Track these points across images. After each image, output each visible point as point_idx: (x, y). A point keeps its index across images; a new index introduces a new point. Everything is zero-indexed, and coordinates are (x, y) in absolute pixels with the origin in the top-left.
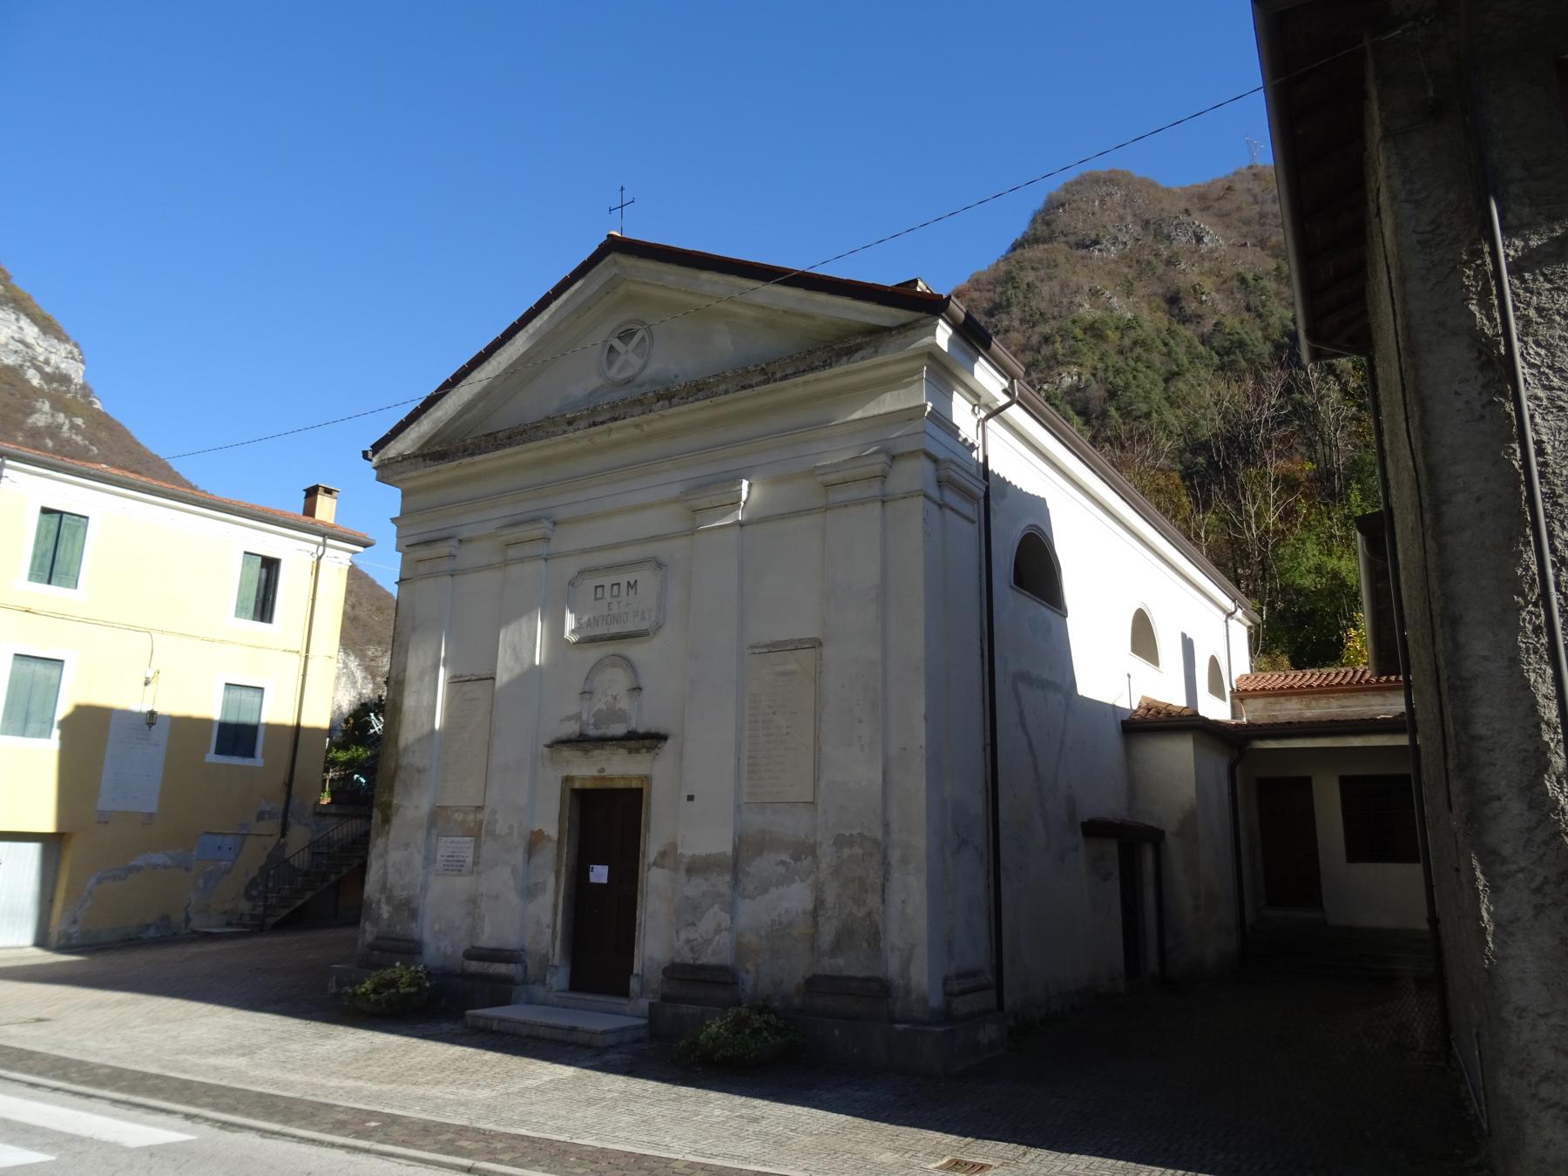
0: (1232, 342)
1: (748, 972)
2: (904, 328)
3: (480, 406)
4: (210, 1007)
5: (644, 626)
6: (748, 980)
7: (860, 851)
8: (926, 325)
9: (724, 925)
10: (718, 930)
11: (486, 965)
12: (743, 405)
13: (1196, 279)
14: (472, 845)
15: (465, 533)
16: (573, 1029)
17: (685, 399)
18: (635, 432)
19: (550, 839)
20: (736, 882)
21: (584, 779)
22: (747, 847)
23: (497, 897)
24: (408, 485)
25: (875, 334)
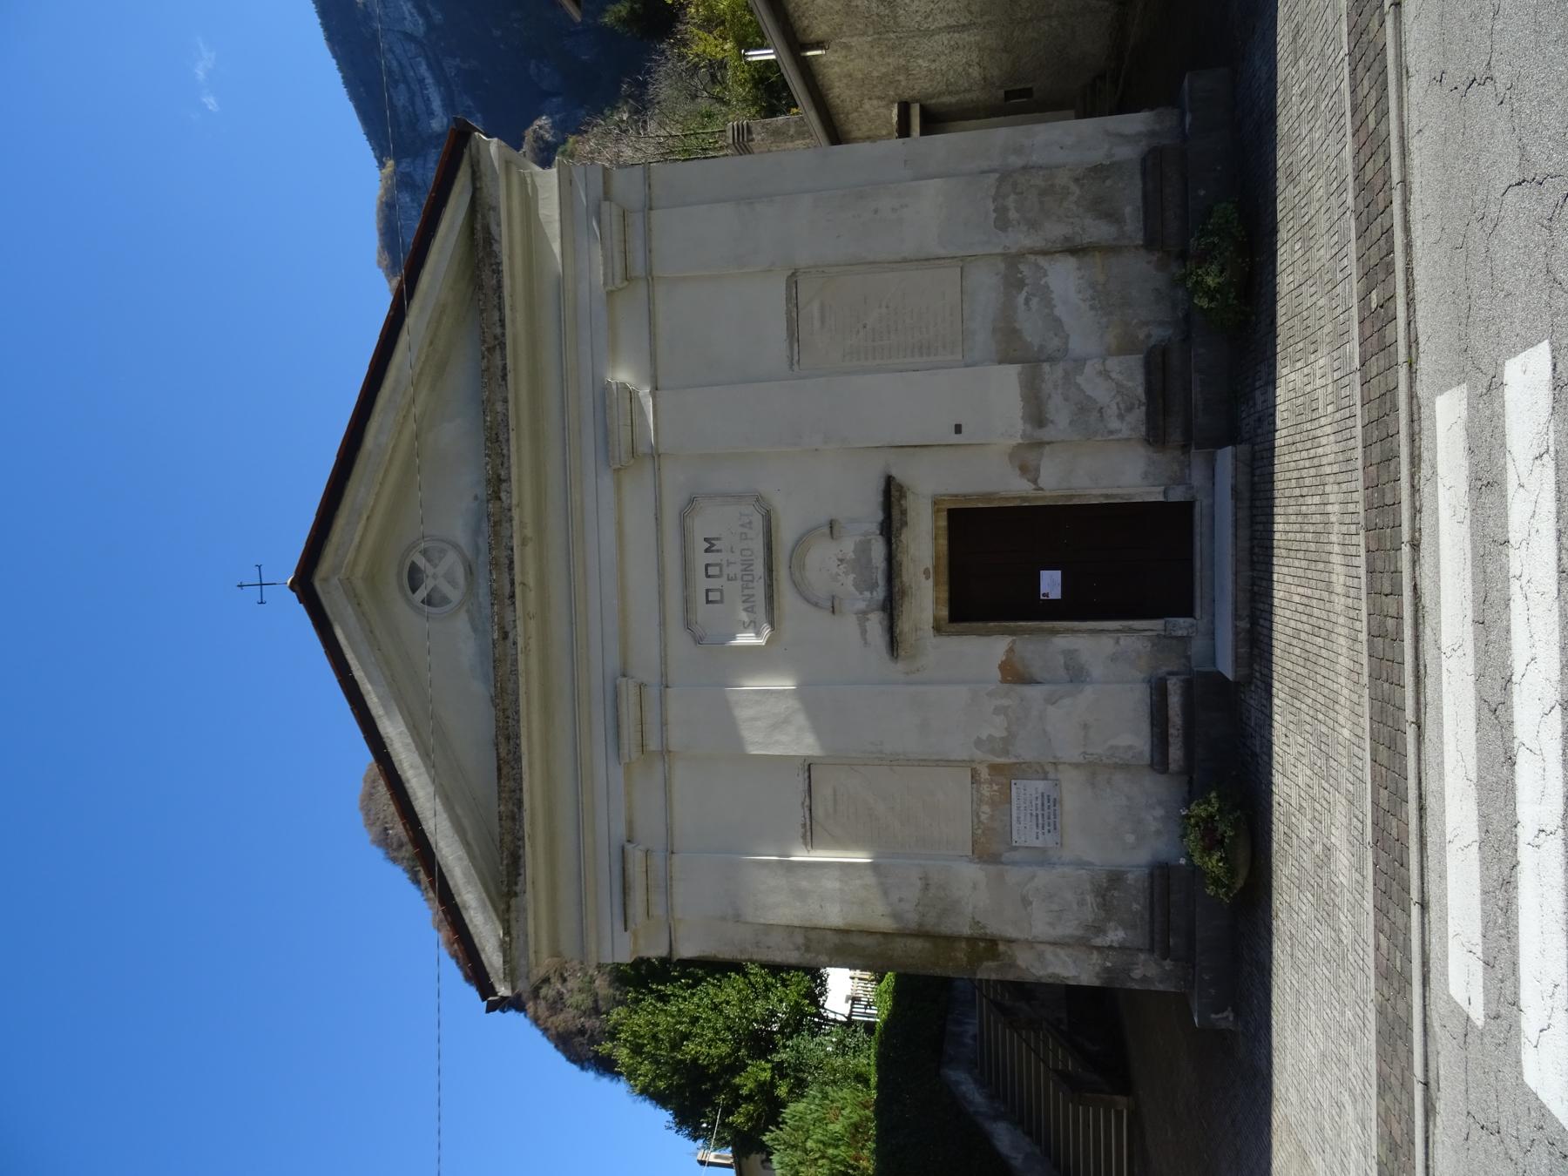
1: (1149, 336)
2: (475, 176)
3: (459, 812)
6: (1159, 334)
7: (1012, 197)
8: (478, 148)
9: (1099, 367)
10: (1105, 374)
11: (1172, 731)
15: (620, 830)
17: (503, 459)
18: (532, 624)
19: (1011, 650)
20: (1051, 360)
21: (937, 601)
22: (1010, 347)
23: (1085, 726)
25: (477, 207)
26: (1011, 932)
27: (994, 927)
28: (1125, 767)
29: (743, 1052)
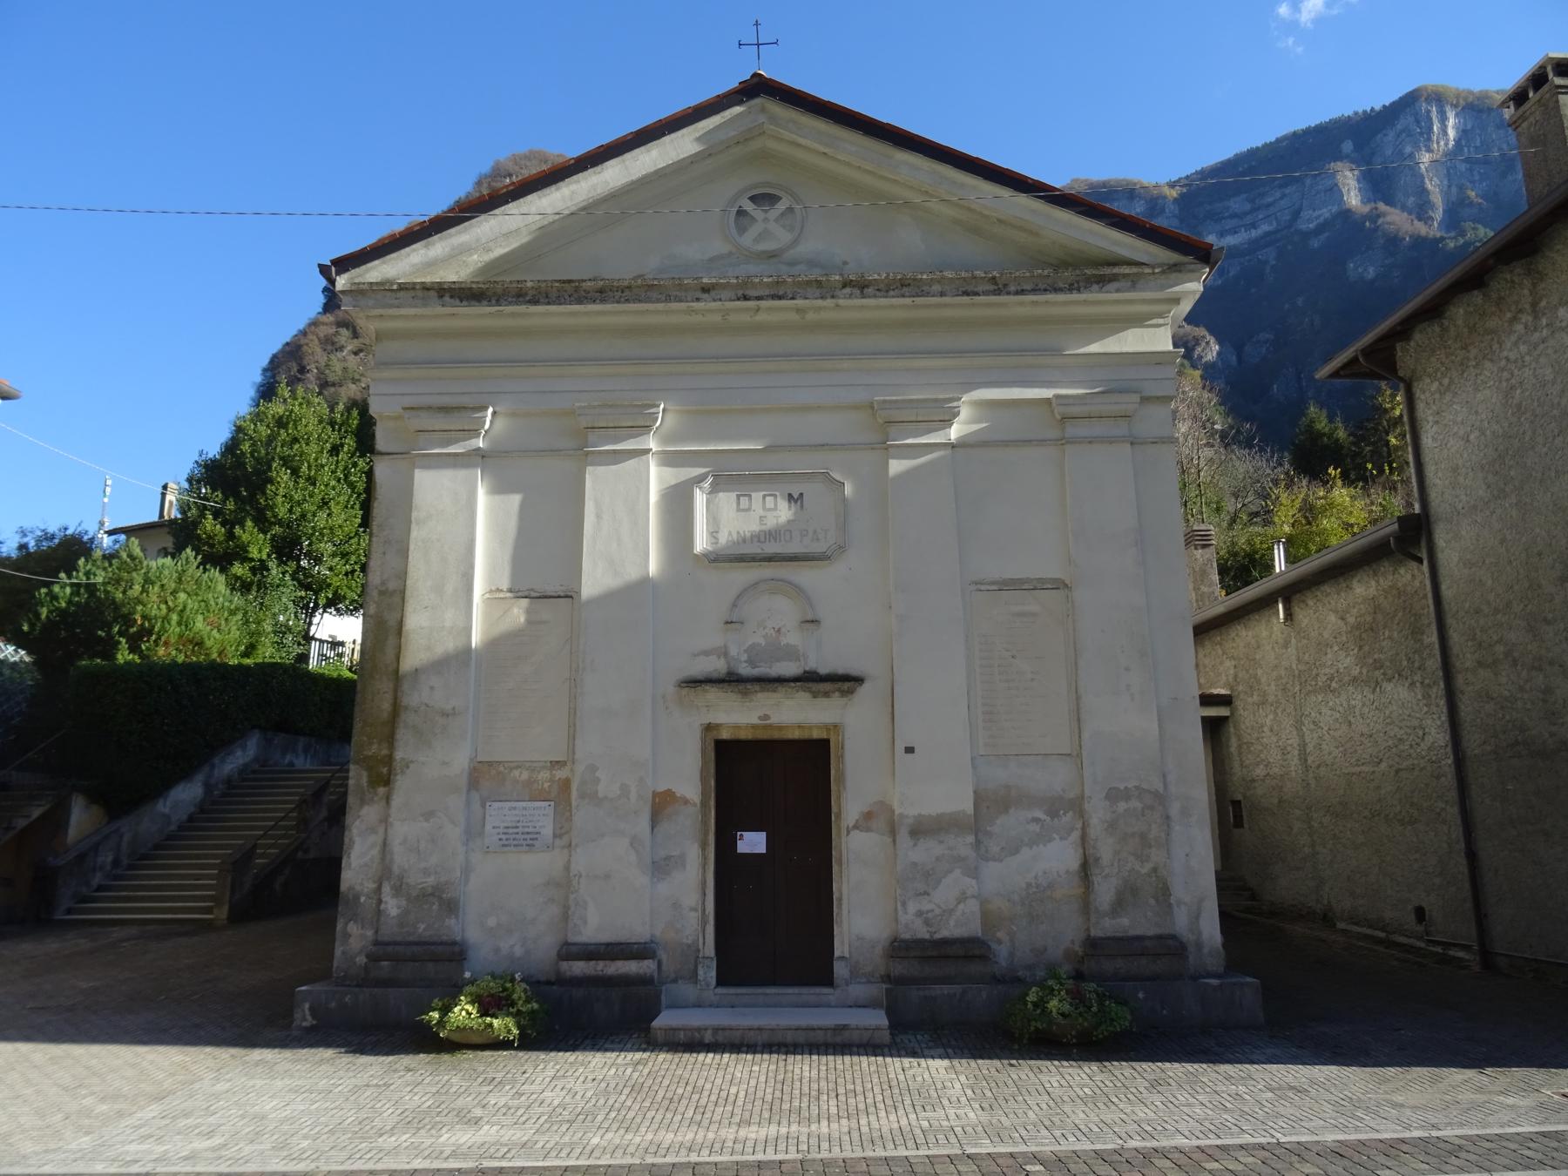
1: (1000, 942)
4: (570, 1057)
6: (1002, 952)
7: (1139, 805)
9: (969, 893)
10: (962, 898)
11: (601, 964)
12: (948, 313)
14: (551, 811)
16: (845, 1027)
18: (717, 318)
19: (686, 802)
21: (737, 727)
22: (991, 803)
23: (607, 877)
27: (402, 783)
28: (566, 916)
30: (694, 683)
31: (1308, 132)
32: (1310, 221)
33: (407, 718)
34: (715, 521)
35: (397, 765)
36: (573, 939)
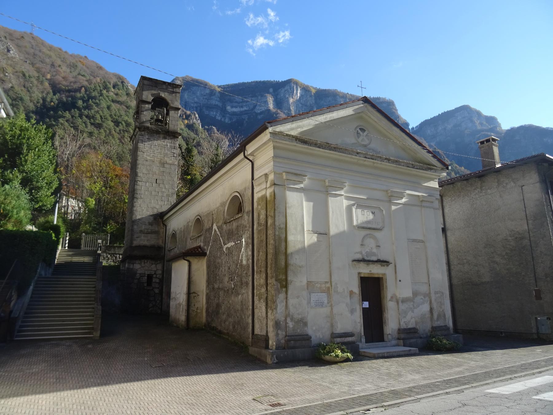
0: (17, 97)
5: (378, 227)
10: (412, 318)
13: (5, 66)
14: (326, 296)
18: (356, 161)
19: (356, 294)
21: (365, 273)
22: (415, 294)
24: (278, 145)
26: (289, 292)
27: (291, 287)
28: (332, 326)
29: (24, 174)
30: (359, 261)
31: (260, 82)
32: (258, 110)
33: (290, 268)
34: (361, 216)
35: (289, 282)
36: (335, 332)
